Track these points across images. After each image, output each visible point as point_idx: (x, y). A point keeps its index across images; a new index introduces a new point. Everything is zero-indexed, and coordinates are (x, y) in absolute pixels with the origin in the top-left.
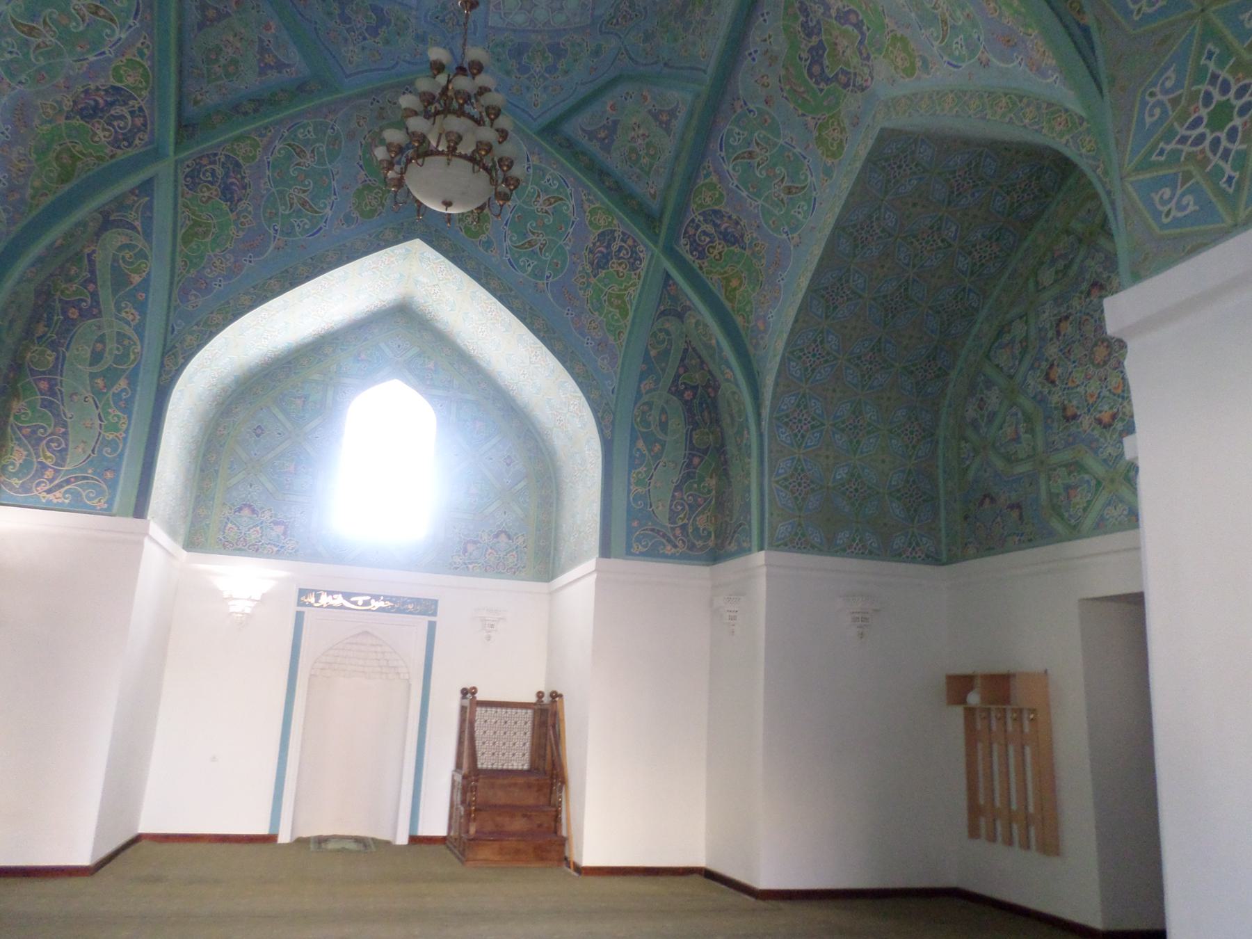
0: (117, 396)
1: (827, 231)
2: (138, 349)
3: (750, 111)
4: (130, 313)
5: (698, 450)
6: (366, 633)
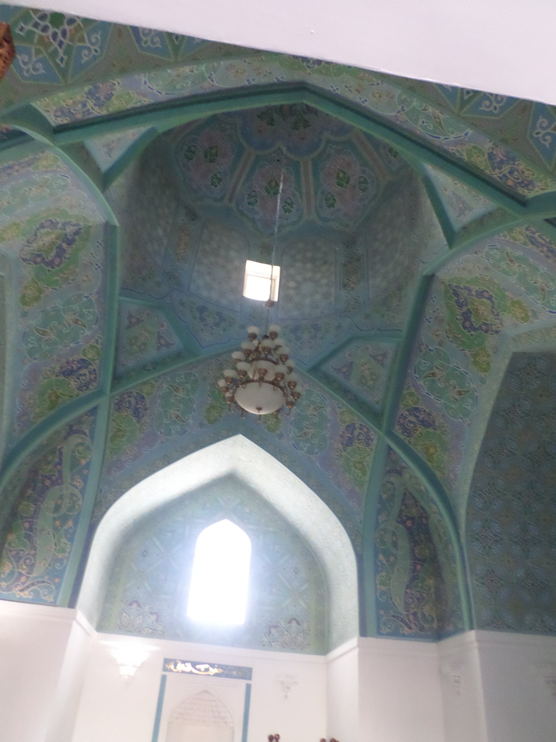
0: (67, 531)
1: (488, 415)
2: (80, 503)
3: (430, 350)
4: (79, 483)
5: (419, 560)
6: (206, 692)
